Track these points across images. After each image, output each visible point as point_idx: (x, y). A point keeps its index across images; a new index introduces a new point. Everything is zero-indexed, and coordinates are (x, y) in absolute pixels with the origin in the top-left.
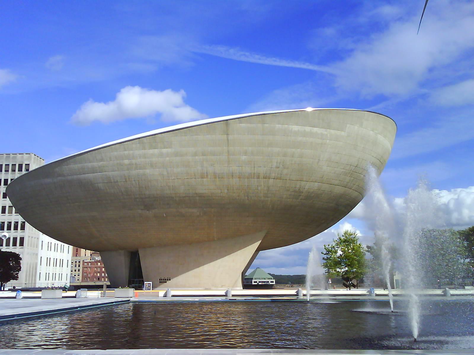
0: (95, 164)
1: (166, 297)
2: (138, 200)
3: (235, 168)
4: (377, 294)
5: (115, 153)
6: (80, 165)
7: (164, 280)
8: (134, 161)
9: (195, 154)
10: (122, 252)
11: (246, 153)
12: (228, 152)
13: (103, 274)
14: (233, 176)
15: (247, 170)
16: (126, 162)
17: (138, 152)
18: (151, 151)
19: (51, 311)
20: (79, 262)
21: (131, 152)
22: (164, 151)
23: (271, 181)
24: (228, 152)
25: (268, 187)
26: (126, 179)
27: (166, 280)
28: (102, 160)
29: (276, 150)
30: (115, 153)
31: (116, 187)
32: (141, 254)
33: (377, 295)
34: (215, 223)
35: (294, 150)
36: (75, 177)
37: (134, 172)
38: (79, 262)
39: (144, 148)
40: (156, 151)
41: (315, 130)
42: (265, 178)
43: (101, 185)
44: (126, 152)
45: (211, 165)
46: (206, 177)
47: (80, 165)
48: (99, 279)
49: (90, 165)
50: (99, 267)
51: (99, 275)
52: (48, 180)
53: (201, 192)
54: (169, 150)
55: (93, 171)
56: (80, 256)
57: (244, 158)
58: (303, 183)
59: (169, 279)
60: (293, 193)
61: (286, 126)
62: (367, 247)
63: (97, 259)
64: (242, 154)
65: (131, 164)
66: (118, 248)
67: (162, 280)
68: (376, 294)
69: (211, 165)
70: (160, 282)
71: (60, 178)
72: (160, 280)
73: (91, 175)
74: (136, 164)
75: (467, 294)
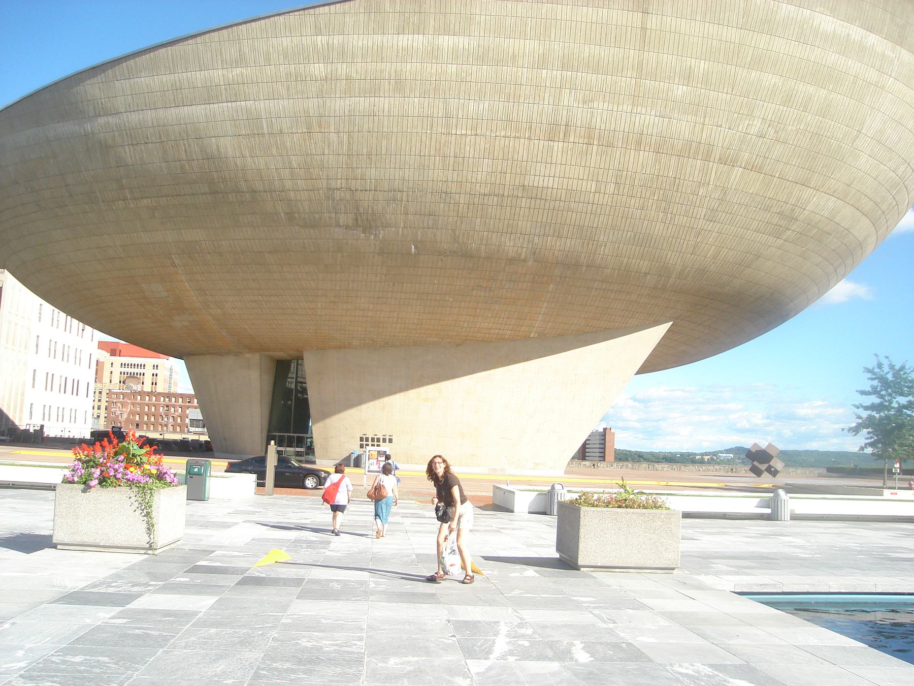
0: (217, 75)
1: (545, 513)
2: (337, 195)
3: (647, 119)
5: (286, 42)
6: (167, 79)
7: (373, 440)
8: (342, 69)
9: (542, 63)
10: (255, 358)
11: (688, 77)
12: (640, 65)
13: (146, 418)
14: (639, 143)
15: (683, 127)
16: (318, 69)
18: (404, 40)
20: (100, 393)
21: (337, 40)
22: (446, 42)
23: (737, 172)
24: (640, 65)
25: (725, 191)
26: (309, 127)
27: (378, 440)
28: (240, 61)
29: (769, 79)
30: (286, 42)
31: (274, 152)
32: (310, 365)
34: (551, 286)
35: (811, 89)
36: (149, 115)
37: (339, 105)
38: (100, 393)
40: (418, 41)
41: (872, 39)
42: (722, 161)
43: (227, 146)
45: (584, 102)
46: (562, 136)
47: (167, 79)
48: (137, 425)
49: (199, 77)
50: (139, 404)
51: (137, 418)
53: (540, 182)
54: (462, 41)
55: (210, 95)
56: (101, 382)
57: (680, 90)
58: (808, 192)
59: (387, 438)
60: (775, 220)
61: (807, 12)
63: (135, 388)
64: (677, 80)
66: (242, 346)
67: (367, 439)
69: (584, 102)
70: (362, 446)
72: (361, 439)
73: (199, 112)
74: (349, 79)
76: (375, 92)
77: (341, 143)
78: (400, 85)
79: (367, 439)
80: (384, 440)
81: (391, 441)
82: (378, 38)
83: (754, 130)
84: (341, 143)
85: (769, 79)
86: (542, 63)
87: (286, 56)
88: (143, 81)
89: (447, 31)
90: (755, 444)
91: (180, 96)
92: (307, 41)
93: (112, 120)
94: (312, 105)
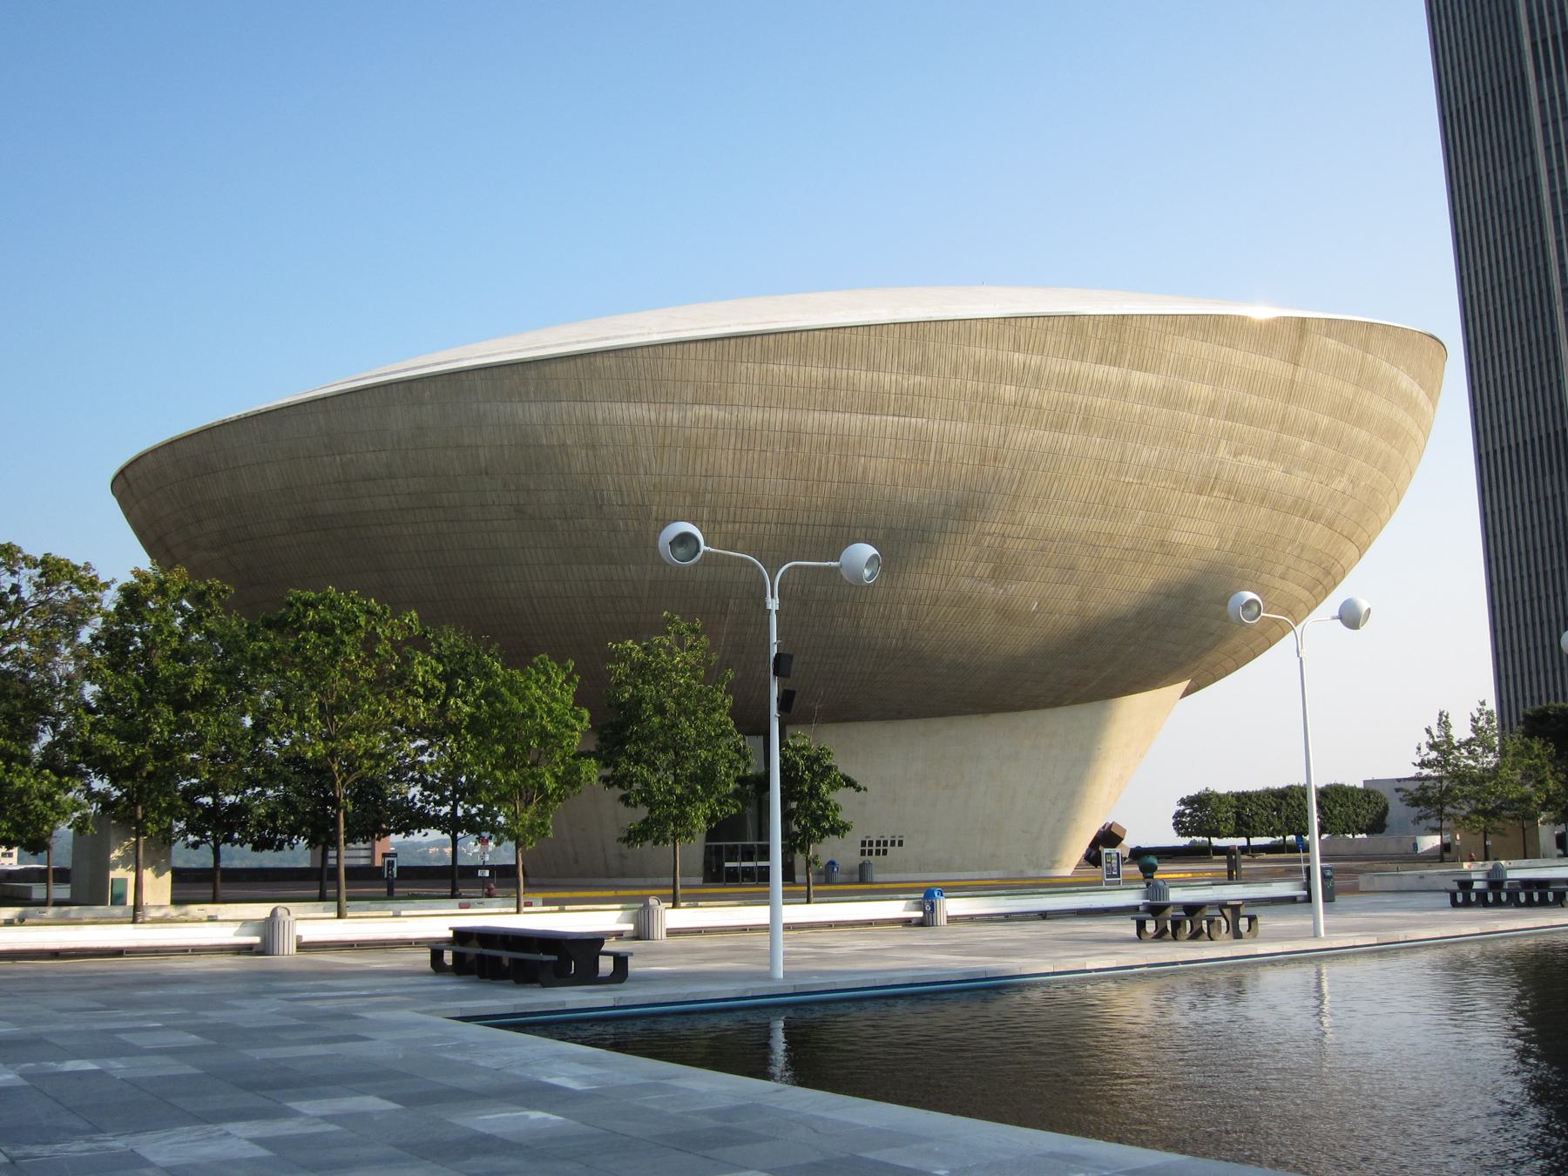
4: (305, 939)
7: (878, 843)
8: (1034, 395)
9: (1211, 410)
11: (1312, 433)
14: (1263, 500)
16: (1008, 392)
17: (1056, 365)
18: (1101, 371)
19: (1354, 954)
21: (1035, 360)
22: (1137, 378)
27: (885, 843)
33: (303, 947)
39: (1081, 355)
40: (1114, 374)
44: (1018, 357)
52: (641, 412)
54: (1151, 379)
55: (873, 404)
62: (609, 786)
65: (1021, 404)
67: (871, 843)
68: (299, 937)
70: (863, 853)
71: (702, 411)
72: (863, 843)
74: (1039, 407)
75: (272, 973)
76: (1060, 425)
77: (1011, 481)
78: (1087, 423)
79: (871, 843)
80: (893, 843)
81: (901, 843)
82: (1076, 365)
83: (1340, 488)
84: (1011, 481)
85: (1362, 435)
86: (1211, 410)
87: (977, 370)
88: (778, 369)
89: (1141, 366)
90: (1124, 831)
91: (831, 399)
92: (1002, 356)
93: (718, 414)
94: (993, 433)
